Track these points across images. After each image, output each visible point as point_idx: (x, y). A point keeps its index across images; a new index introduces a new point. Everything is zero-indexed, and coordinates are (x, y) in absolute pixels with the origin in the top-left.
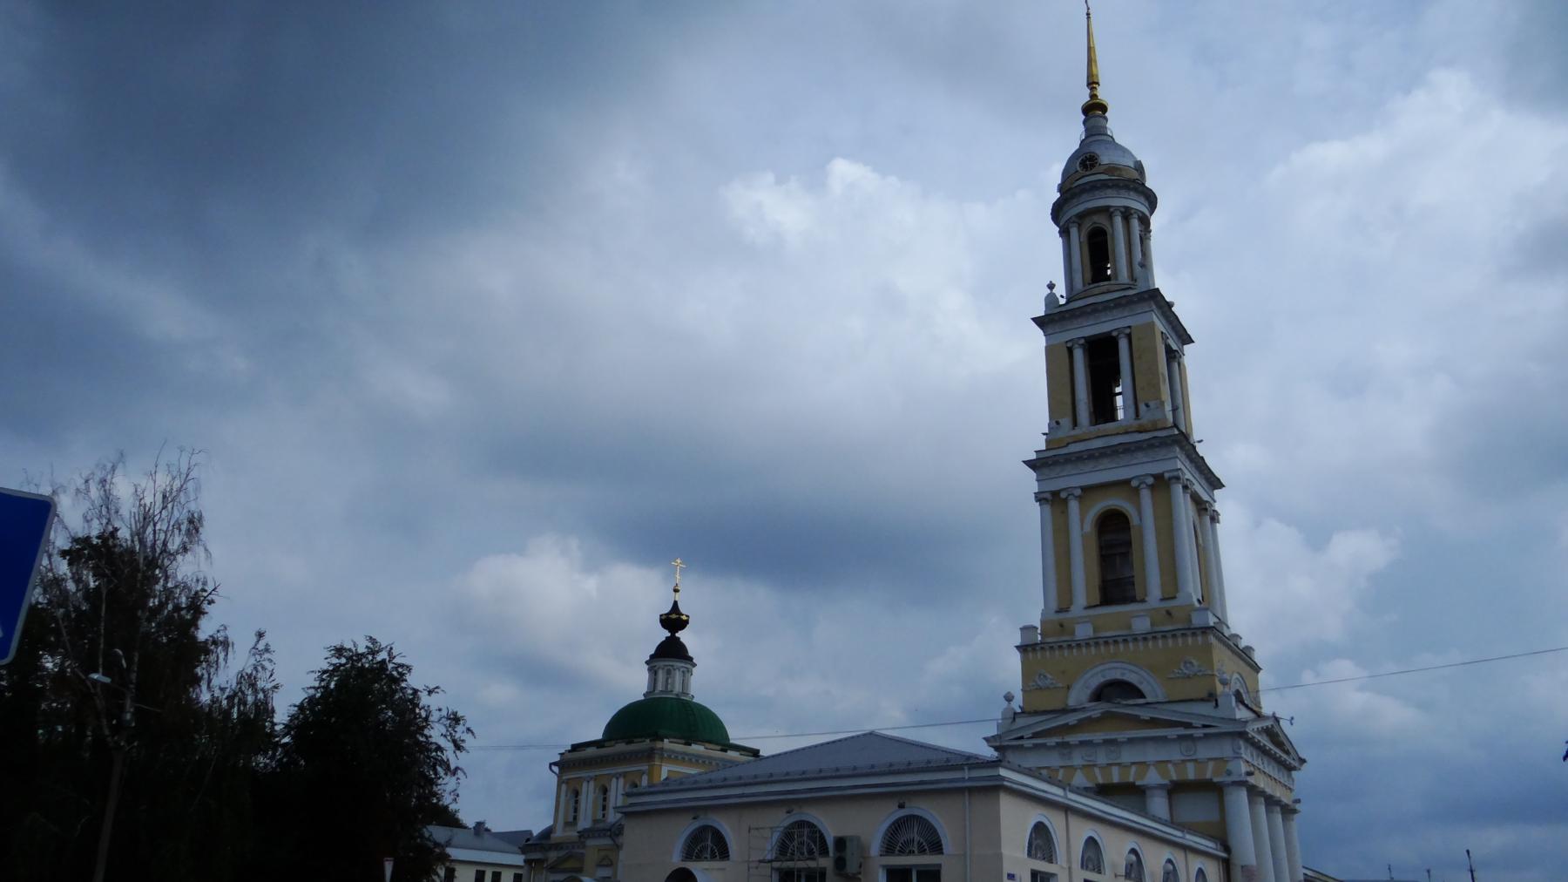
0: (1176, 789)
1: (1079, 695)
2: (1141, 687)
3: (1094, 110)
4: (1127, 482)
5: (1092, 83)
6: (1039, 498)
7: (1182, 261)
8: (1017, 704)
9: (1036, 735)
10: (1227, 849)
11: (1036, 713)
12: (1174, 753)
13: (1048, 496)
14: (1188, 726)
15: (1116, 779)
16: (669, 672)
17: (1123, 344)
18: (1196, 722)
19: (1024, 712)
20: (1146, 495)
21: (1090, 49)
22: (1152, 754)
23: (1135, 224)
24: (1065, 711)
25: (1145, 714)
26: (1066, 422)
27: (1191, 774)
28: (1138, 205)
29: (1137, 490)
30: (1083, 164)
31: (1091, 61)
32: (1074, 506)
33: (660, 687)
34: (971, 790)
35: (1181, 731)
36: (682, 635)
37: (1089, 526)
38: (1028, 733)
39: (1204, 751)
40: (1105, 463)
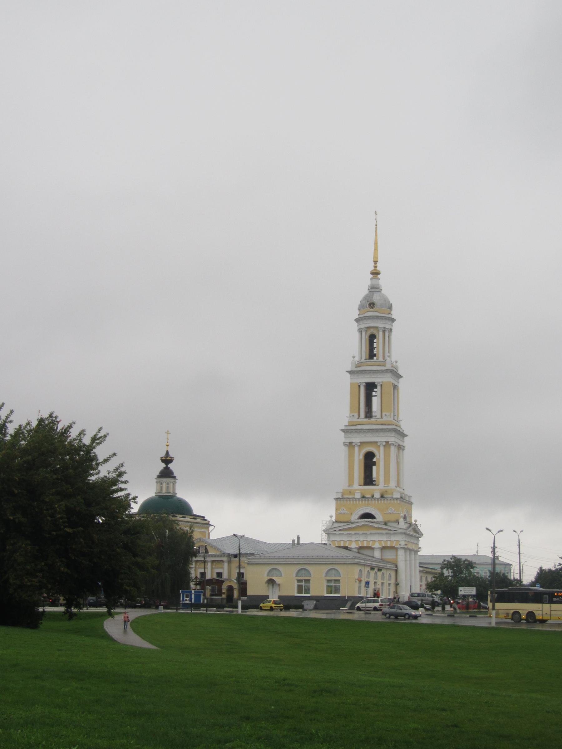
0: (384, 548)
1: (355, 517)
2: (375, 515)
3: (375, 273)
4: (377, 442)
5: (376, 262)
6: (345, 444)
7: (401, 348)
8: (334, 519)
9: (340, 530)
10: (397, 566)
11: (341, 522)
12: (384, 538)
13: (348, 444)
14: (389, 530)
15: (365, 545)
16: (168, 484)
17: (379, 387)
18: (392, 529)
19: (336, 522)
20: (382, 448)
21: (376, 244)
22: (376, 538)
23: (387, 334)
24: (349, 522)
25: (376, 525)
26: (356, 415)
27: (389, 544)
28: (392, 438)
29: (379, 446)
30: (370, 305)
31: (376, 249)
32: (356, 449)
33: (164, 490)
34: (348, 564)
35: (387, 532)
36: (170, 465)
37: (362, 457)
38: (338, 529)
39: (393, 538)
40: (369, 435)
